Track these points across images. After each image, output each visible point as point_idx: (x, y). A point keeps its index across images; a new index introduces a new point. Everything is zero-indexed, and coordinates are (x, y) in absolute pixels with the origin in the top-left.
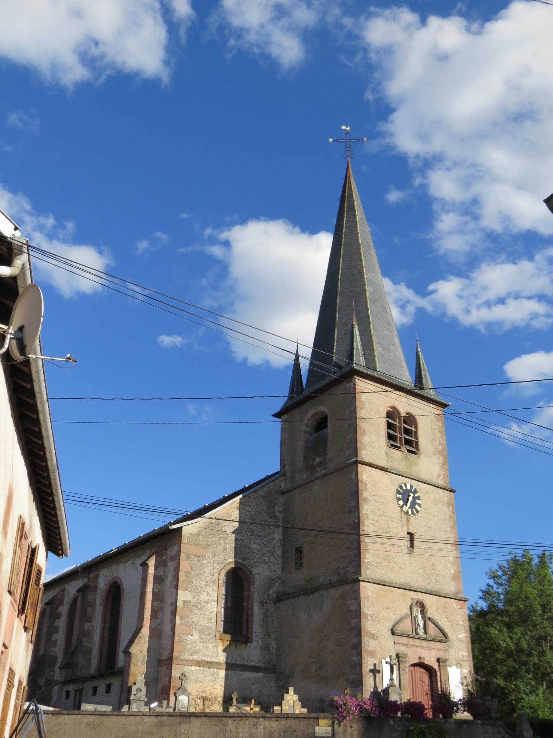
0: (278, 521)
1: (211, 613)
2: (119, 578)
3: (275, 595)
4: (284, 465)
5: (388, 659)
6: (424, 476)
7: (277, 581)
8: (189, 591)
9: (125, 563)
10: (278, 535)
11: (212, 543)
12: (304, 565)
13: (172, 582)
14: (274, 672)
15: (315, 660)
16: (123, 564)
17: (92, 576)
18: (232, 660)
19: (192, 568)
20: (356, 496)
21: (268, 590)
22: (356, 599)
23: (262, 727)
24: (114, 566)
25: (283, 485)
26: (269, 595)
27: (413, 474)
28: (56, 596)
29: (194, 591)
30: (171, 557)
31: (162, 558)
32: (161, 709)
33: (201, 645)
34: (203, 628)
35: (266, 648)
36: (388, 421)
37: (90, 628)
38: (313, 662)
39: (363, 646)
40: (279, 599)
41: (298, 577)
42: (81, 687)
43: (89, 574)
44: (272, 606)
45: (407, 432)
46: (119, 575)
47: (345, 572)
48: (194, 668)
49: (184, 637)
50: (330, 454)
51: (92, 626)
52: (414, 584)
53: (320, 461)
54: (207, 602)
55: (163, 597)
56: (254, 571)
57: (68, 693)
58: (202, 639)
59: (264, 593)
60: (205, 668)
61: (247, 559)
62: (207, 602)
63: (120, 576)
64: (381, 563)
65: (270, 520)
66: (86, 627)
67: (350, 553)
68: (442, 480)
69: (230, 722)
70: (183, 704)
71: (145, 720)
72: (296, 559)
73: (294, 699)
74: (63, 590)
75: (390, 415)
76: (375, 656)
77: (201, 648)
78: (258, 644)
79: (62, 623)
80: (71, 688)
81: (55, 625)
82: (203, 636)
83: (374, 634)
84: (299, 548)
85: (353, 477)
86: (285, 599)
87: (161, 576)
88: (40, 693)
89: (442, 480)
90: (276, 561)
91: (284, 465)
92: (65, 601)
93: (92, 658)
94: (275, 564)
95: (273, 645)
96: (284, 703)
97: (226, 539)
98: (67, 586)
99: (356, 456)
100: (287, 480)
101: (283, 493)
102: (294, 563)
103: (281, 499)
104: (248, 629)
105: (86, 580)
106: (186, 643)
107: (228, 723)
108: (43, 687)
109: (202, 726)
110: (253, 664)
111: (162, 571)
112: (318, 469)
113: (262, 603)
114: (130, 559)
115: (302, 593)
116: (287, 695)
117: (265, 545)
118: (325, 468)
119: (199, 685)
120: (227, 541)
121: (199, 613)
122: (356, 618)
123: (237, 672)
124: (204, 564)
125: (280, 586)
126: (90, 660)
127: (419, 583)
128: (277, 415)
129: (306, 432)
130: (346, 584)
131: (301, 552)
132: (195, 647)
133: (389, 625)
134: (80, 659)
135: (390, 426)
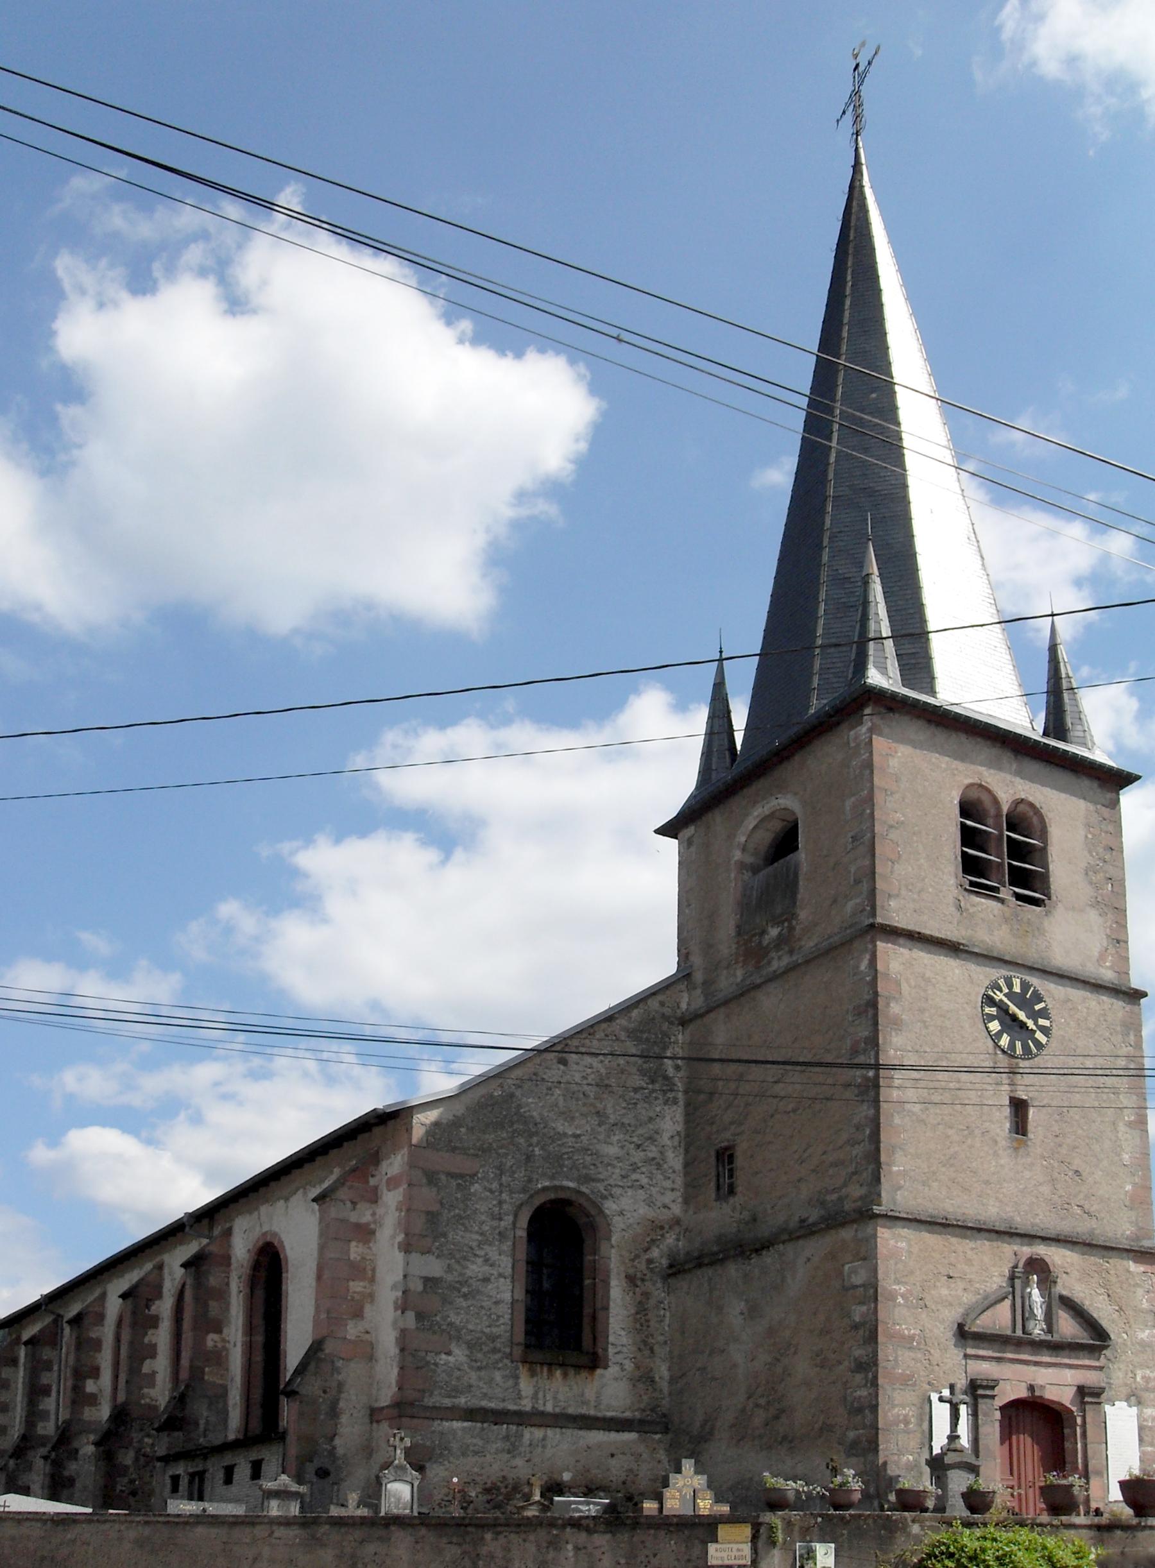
0: (671, 1090)
1: (497, 1303)
2: (275, 1234)
3: (665, 1262)
4: (688, 954)
5: (946, 1393)
6: (1060, 959)
7: (670, 1228)
8: (438, 1257)
9: (287, 1199)
10: (671, 1122)
11: (494, 1145)
12: (739, 1189)
13: (393, 1237)
14: (666, 1430)
15: (762, 1401)
16: (282, 1202)
17: (217, 1231)
18: (554, 1407)
19: (441, 1204)
20: (871, 1013)
21: (647, 1250)
22: (864, 1259)
23: (570, 1547)
24: (264, 1209)
25: (686, 1001)
26: (650, 1261)
27: (1032, 956)
28: (141, 1280)
29: (451, 1255)
30: (389, 1181)
31: (368, 1182)
32: (343, 1509)
33: (473, 1375)
34: (479, 1339)
35: (644, 1378)
36: (963, 825)
37: (219, 1345)
38: (757, 1406)
39: (882, 1364)
40: (676, 1269)
41: (720, 1218)
42: (200, 1468)
43: (211, 1228)
44: (659, 1285)
45: (1018, 850)
46: (275, 1228)
47: (841, 1199)
48: (456, 1425)
49: (428, 1358)
50: (803, 914)
51: (224, 1340)
52: (1022, 1222)
53: (780, 934)
54: (486, 1280)
55: (374, 1270)
56: (610, 1207)
57: (175, 1479)
58: (476, 1361)
59: (637, 1256)
60: (485, 1425)
61: (588, 1179)
62: (486, 1280)
63: (277, 1230)
64: (934, 1173)
65: (650, 1086)
66: (210, 1344)
67: (854, 1153)
68: (1111, 968)
69: (488, 1536)
70: (399, 1500)
71: (276, 1534)
72: (718, 1175)
73: (697, 1486)
74: (160, 1267)
75: (968, 809)
76: (915, 1385)
77: (473, 1382)
78: (623, 1370)
79: (162, 1337)
80: (180, 1469)
81: (146, 1340)
82: (479, 1356)
83: (912, 1338)
84: (727, 1149)
85: (864, 965)
86: (690, 1270)
87: (368, 1224)
88: (126, 1480)
89: (1111, 968)
90: (668, 1184)
91: (688, 954)
92: (165, 1290)
93: (230, 1409)
94: (665, 1189)
95: (662, 1371)
96: (668, 1493)
97: (532, 1135)
98: (166, 1258)
99: (874, 915)
100: (695, 988)
101: (684, 1022)
102: (713, 1184)
103: (681, 1037)
104: (595, 1339)
105: (205, 1241)
106: (434, 1371)
107: (483, 1538)
108: (131, 1470)
109: (418, 1547)
110: (609, 1414)
111: (368, 1213)
112: (773, 954)
113: (631, 1280)
114: (297, 1190)
115: (732, 1253)
116: (678, 1476)
117: (638, 1146)
118: (791, 952)
119: (472, 1460)
120: (535, 1140)
121: (464, 1304)
122: (863, 1303)
123: (569, 1432)
124: (474, 1194)
125: (678, 1240)
126: (226, 1413)
127: (1044, 1219)
128: (668, 830)
129: (742, 866)
130: (843, 1225)
131: (731, 1158)
132: (458, 1378)
133: (952, 1315)
134: (201, 1411)
135: (969, 837)
